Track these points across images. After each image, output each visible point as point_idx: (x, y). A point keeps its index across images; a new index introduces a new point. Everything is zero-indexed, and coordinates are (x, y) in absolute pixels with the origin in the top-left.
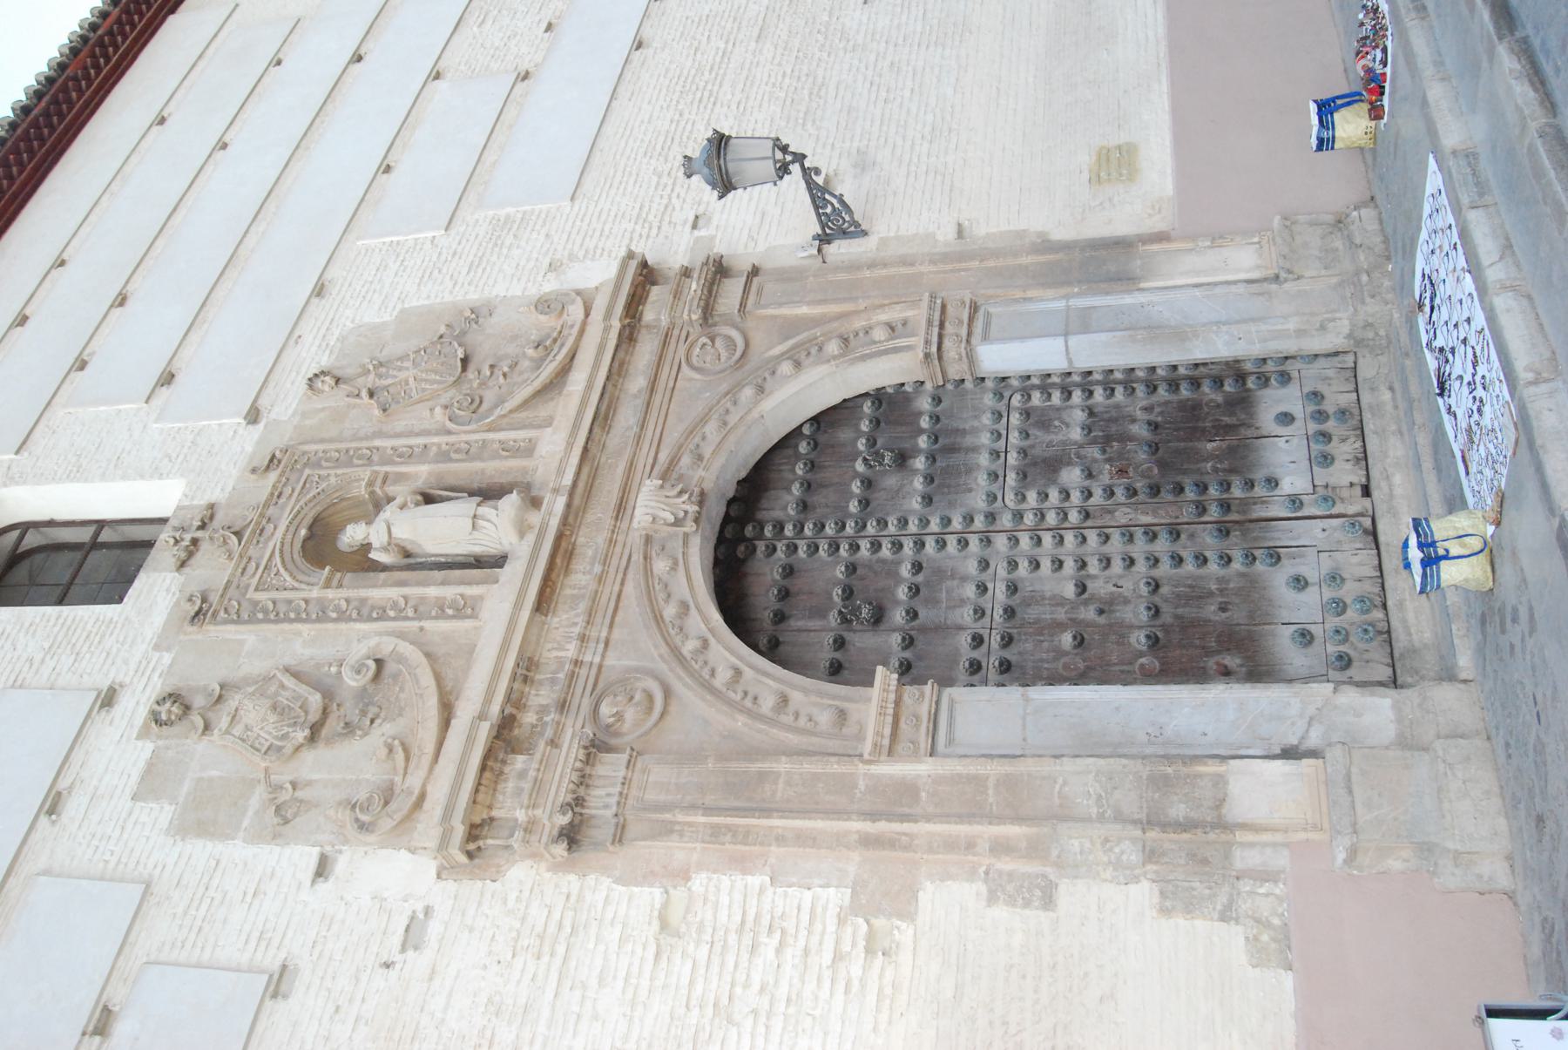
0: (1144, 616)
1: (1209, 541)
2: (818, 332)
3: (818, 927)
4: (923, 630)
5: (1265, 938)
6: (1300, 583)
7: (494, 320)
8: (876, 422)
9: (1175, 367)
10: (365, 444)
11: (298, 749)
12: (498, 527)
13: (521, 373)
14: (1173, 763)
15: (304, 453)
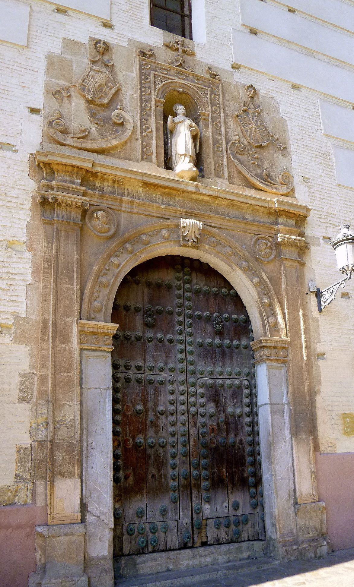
0: (150, 441)
1: (183, 469)
2: (273, 292)
3: (11, 304)
4: (144, 344)
5: (10, 494)
6: (164, 512)
7: (280, 157)
8: (236, 321)
9: (259, 454)
10: (222, 110)
11: (84, 97)
12: (184, 166)
13: (255, 170)
14: (79, 454)
15: (218, 87)
